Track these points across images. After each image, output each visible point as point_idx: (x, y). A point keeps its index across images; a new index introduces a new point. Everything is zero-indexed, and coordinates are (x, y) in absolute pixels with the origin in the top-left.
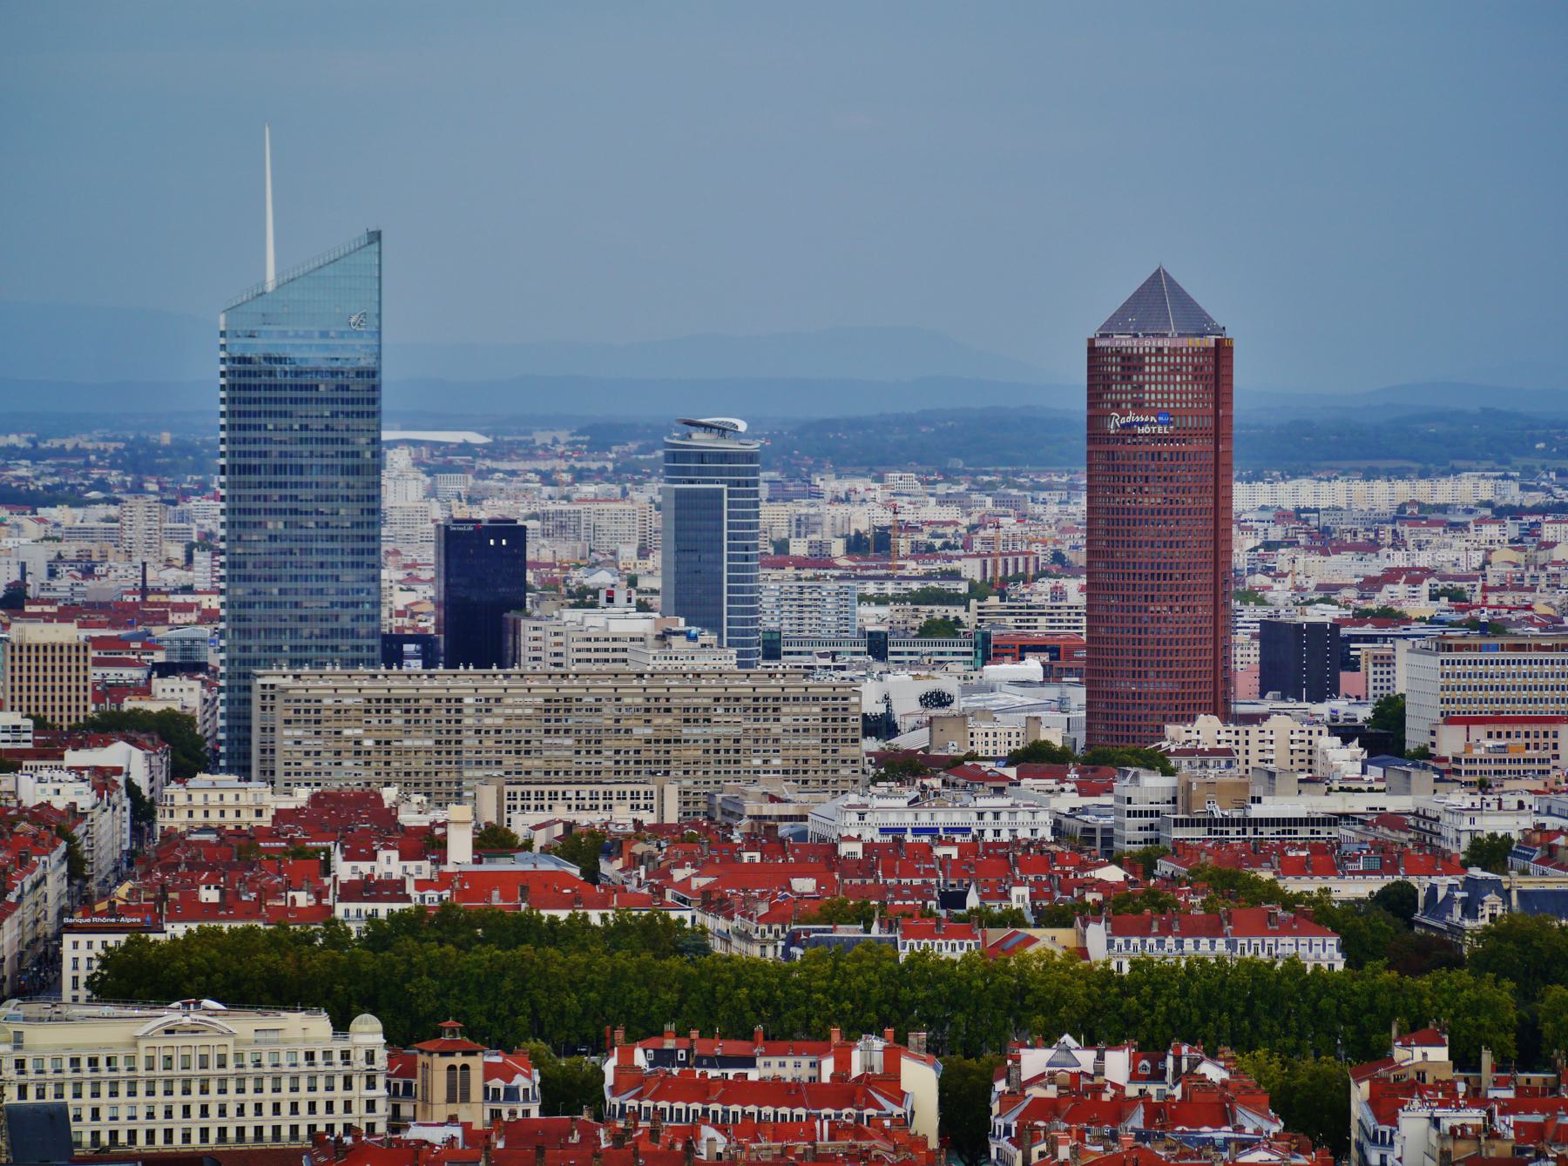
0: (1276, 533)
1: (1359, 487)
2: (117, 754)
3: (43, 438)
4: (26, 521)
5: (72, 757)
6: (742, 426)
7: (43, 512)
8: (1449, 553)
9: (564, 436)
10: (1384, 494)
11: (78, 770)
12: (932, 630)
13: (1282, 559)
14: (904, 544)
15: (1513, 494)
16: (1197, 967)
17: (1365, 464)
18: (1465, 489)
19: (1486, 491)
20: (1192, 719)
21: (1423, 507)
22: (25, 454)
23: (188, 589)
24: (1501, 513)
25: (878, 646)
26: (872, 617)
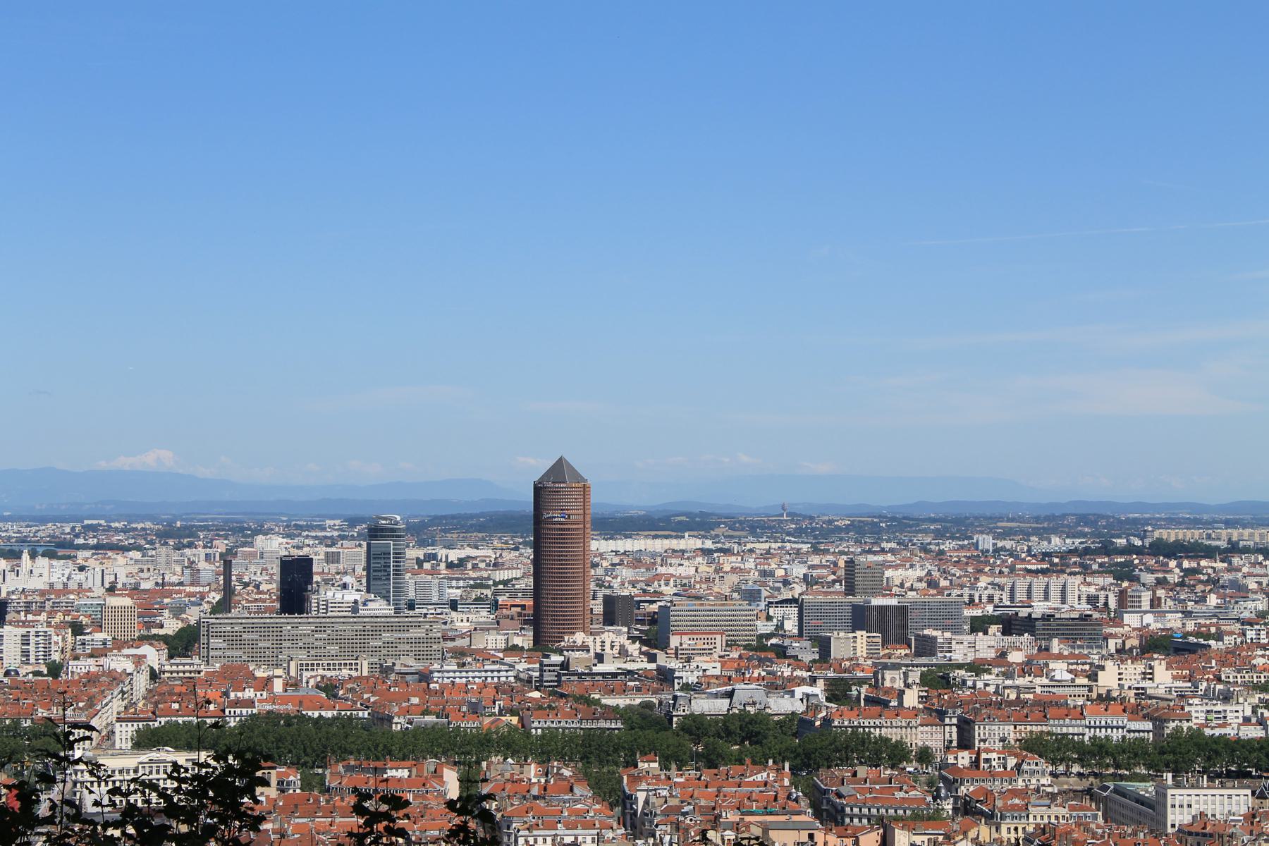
20: (574, 633)
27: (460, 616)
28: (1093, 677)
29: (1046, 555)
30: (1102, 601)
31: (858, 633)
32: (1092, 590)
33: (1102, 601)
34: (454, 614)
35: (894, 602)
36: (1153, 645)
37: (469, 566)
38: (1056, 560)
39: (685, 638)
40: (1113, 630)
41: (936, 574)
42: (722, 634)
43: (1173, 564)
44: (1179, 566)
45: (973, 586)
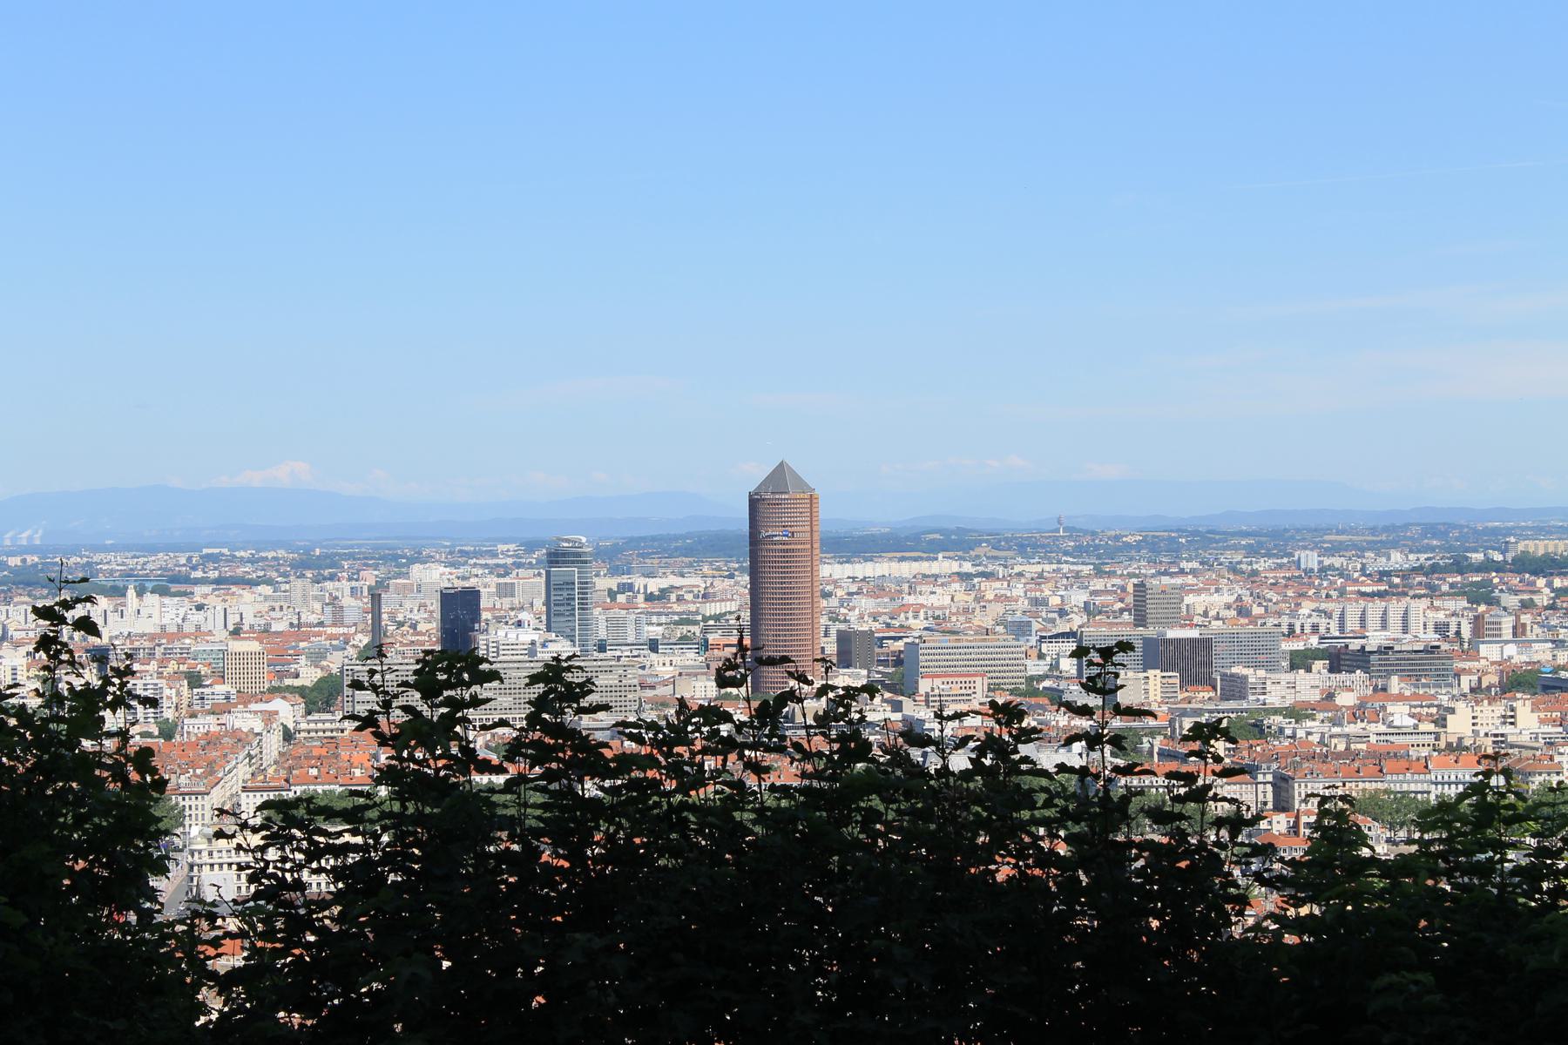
0: (854, 588)
1: (894, 565)
2: (278, 704)
3: (258, 551)
4: (245, 593)
5: (253, 707)
6: (584, 540)
7: (1461, 788)
8: (939, 599)
9: (512, 547)
10: (907, 569)
11: (256, 712)
12: (684, 639)
13: (856, 600)
14: (673, 597)
15: (967, 567)
16: (155, 795)
17: (899, 555)
18: (944, 565)
19: (955, 567)
21: (925, 576)
22: (249, 561)
23: (321, 624)
24: (964, 577)
25: (653, 646)
26: (655, 631)
27: (661, 659)
28: (1441, 722)
29: (1384, 575)
30: (1453, 629)
31: (1151, 673)
32: (1441, 616)
33: (1453, 629)
34: (653, 656)
35: (1194, 634)
36: (1517, 682)
37: (673, 597)
38: (1397, 580)
39: (938, 682)
40: (1467, 665)
41: (1247, 599)
42: (983, 676)
43: (1541, 582)
44: (1549, 585)
45: (1293, 614)
